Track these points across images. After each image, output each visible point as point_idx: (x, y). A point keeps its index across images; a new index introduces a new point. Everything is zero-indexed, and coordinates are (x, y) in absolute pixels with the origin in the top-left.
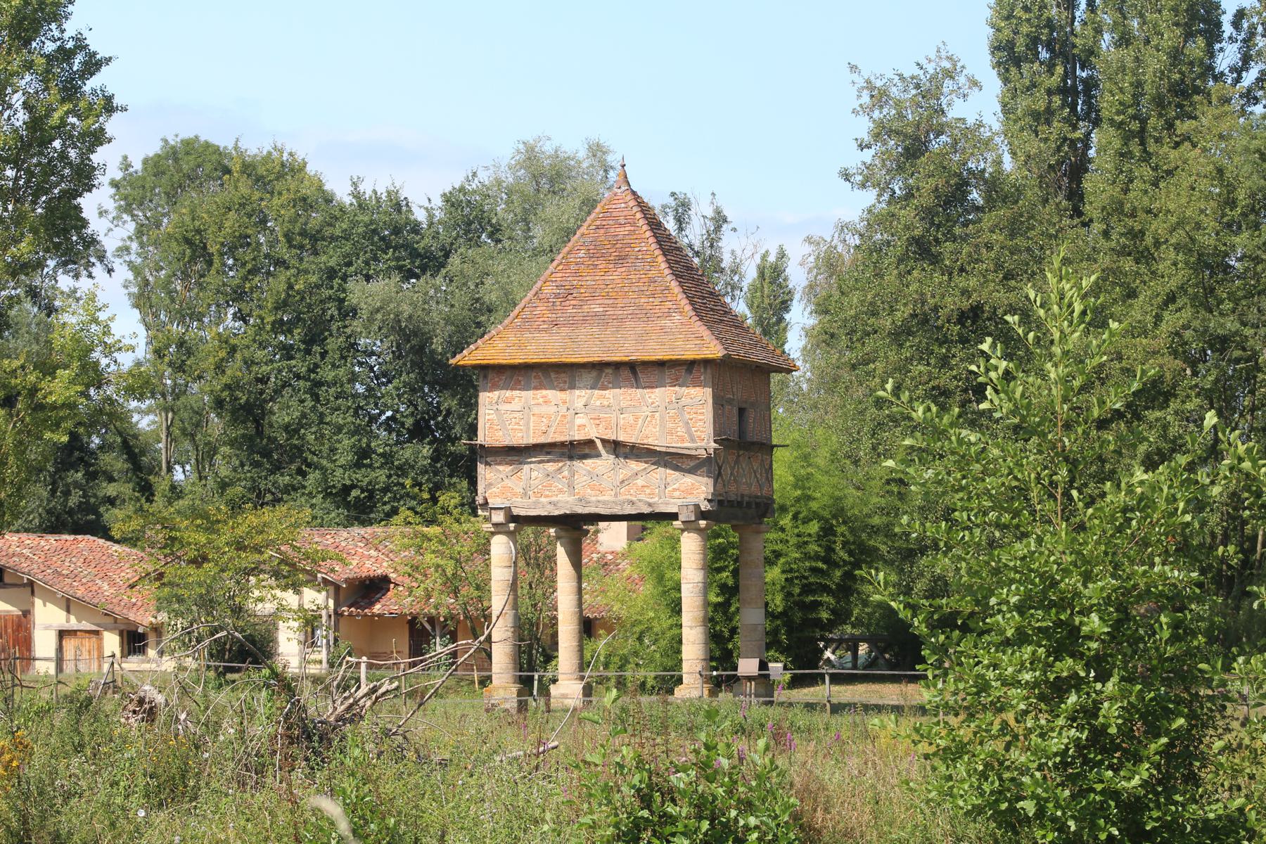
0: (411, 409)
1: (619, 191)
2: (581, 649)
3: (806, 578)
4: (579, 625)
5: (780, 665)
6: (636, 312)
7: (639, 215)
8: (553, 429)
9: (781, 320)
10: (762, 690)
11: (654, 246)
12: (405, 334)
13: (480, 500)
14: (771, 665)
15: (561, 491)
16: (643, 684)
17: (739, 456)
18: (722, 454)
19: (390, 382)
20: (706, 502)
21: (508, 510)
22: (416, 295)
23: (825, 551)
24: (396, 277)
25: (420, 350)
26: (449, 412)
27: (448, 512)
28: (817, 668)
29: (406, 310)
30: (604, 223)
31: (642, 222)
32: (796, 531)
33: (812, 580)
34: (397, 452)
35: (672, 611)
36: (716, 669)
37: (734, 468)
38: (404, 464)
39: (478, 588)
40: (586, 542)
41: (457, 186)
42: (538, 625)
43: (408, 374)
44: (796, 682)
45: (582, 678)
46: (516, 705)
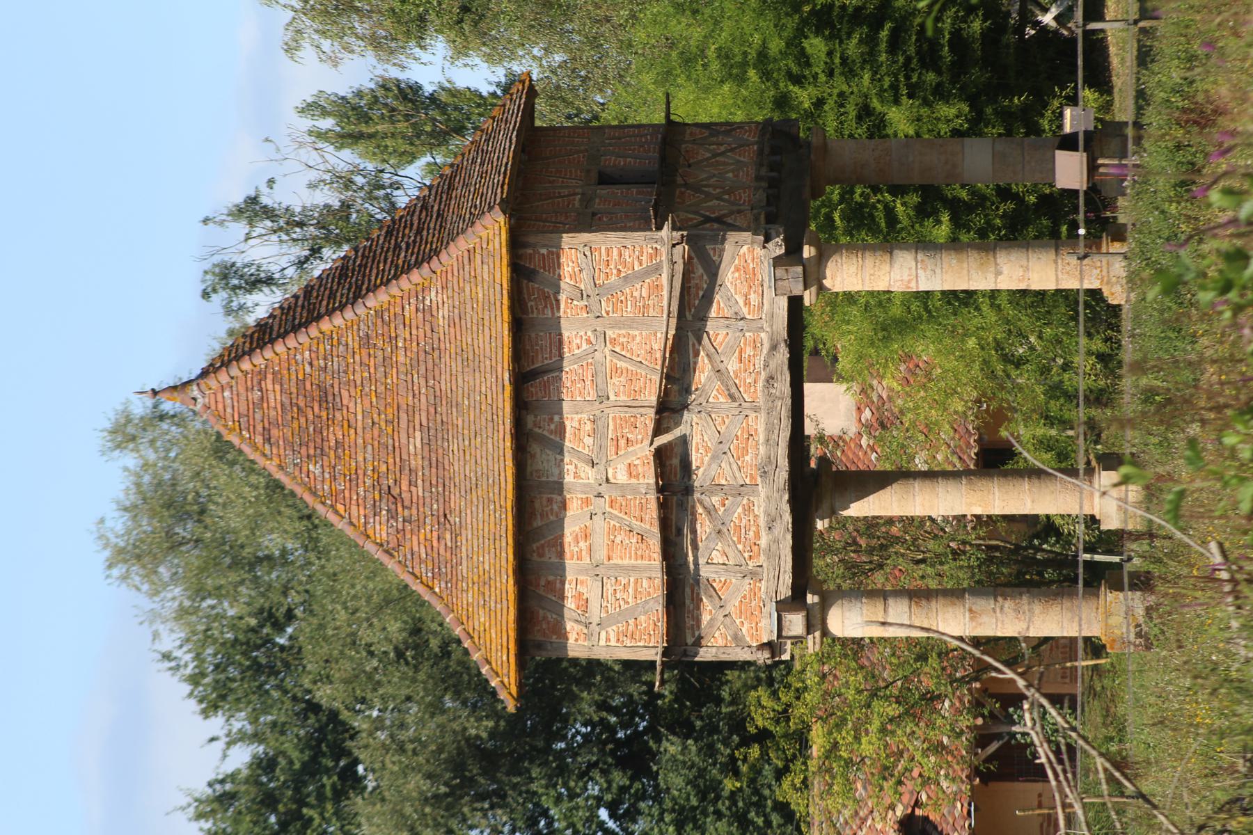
0: (596, 774)
1: (200, 400)
2: (1035, 474)
3: (908, 60)
4: (991, 476)
5: (1068, 112)
6: (422, 371)
7: (246, 365)
8: (636, 524)
9: (433, 98)
10: (1114, 144)
11: (302, 338)
12: (461, 786)
13: (763, 657)
14: (1068, 129)
15: (748, 510)
16: (1101, 357)
17: (686, 185)
18: (683, 215)
19: (545, 813)
20: (770, 245)
21: (783, 607)
22: (389, 765)
23: (860, 25)
24: (358, 803)
25: (488, 758)
26: (603, 706)
27: (785, 711)
28: (1073, 41)
29: (416, 784)
30: (259, 428)
31: (258, 360)
32: (822, 78)
33: (912, 50)
34: (673, 799)
35: (966, 305)
36: (1074, 226)
37: (708, 195)
38: (695, 786)
39: (922, 658)
40: (843, 460)
41: (187, 688)
42: (989, 547)
43: (532, 780)
44: (1100, 78)
45: (1090, 472)
46: (1139, 593)
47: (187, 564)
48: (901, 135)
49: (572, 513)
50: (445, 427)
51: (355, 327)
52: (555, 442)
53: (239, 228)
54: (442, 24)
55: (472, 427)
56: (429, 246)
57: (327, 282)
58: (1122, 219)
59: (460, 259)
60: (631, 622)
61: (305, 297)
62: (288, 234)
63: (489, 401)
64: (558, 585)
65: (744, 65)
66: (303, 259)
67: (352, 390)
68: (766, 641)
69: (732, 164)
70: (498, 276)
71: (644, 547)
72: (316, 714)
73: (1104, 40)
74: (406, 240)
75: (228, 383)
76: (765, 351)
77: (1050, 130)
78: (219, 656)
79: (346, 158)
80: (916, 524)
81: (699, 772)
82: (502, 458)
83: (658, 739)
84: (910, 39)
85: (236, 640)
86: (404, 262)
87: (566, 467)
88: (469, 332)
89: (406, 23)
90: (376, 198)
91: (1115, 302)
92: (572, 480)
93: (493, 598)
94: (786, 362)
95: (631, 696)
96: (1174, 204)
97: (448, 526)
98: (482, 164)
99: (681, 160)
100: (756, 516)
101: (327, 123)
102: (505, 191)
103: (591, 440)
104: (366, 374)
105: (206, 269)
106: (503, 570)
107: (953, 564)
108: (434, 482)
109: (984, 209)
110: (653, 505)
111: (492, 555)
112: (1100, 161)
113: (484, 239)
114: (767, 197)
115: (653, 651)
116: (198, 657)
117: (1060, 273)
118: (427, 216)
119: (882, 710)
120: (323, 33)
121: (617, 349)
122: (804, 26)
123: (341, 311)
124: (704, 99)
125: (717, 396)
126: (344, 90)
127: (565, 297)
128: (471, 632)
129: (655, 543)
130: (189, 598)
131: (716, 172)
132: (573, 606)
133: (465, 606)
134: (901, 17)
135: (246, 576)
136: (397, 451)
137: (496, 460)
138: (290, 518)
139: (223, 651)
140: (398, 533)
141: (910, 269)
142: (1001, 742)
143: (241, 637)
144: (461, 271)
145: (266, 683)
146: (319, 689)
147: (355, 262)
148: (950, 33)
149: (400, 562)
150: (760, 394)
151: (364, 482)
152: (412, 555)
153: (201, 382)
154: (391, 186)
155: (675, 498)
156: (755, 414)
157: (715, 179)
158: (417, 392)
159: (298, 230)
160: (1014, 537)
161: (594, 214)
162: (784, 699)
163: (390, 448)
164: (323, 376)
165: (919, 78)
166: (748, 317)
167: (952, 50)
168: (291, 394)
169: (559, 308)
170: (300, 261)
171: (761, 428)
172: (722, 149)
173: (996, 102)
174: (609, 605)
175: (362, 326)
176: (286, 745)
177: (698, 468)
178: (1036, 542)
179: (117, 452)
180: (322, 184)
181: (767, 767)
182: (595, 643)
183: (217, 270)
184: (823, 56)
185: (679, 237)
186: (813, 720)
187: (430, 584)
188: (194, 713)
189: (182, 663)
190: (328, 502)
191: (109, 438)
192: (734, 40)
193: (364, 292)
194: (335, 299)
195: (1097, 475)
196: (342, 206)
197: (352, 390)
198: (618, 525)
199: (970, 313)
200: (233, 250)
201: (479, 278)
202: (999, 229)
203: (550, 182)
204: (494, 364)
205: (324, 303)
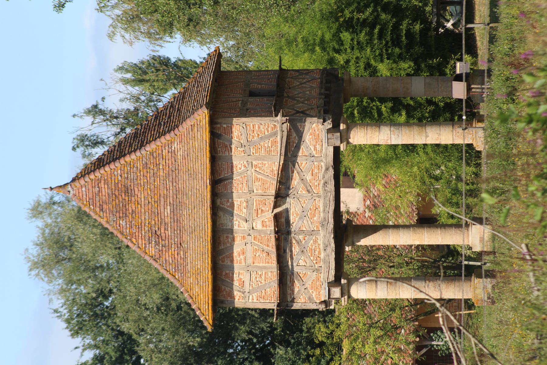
1: (72, 192)
2: (444, 226)
3: (387, 42)
4: (423, 227)
5: (458, 64)
6: (171, 179)
7: (92, 176)
8: (265, 248)
9: (175, 65)
10: (479, 79)
11: (117, 164)
13: (322, 307)
14: (458, 72)
15: (315, 241)
17: (288, 97)
18: (287, 110)
20: (326, 124)
21: (331, 285)
22: (154, 359)
23: (366, 27)
26: (250, 333)
27: (331, 333)
30: (98, 204)
31: (98, 174)
32: (349, 50)
33: (389, 38)
35: (413, 152)
36: (460, 117)
37: (298, 101)
39: (393, 310)
40: (357, 221)
41: (65, 325)
44: (472, 50)
45: (467, 225)
46: (489, 280)
47: (65, 269)
48: (384, 76)
49: (237, 243)
50: (181, 204)
51: (141, 159)
52: (230, 211)
53: (89, 119)
54: (180, 27)
55: (193, 204)
56: (174, 123)
57: (128, 140)
58: (482, 113)
59: (188, 129)
60: (263, 291)
61: (118, 146)
62: (111, 122)
63: (201, 193)
64: (231, 275)
65: (314, 44)
66: (117, 133)
67: (139, 188)
68: (323, 300)
69: (309, 88)
70: (204, 137)
71: (269, 258)
72: (122, 336)
73: (474, 34)
74: (163, 121)
75: (84, 184)
76: (323, 171)
77: (450, 74)
78: (79, 310)
79: (136, 90)
80: (390, 250)
81: (293, 363)
82: (206, 218)
83: (275, 348)
84: (388, 33)
85: (87, 303)
86: (163, 131)
87: (235, 222)
88: (192, 161)
89: (164, 26)
90: (150, 106)
91: (479, 150)
92: (237, 228)
93: (202, 280)
94: (333, 176)
95: (263, 328)
96: (505, 105)
97: (182, 248)
98: (198, 87)
99: (286, 85)
100: (319, 244)
101: (129, 76)
102: (208, 99)
103: (246, 210)
104: (146, 181)
105: (74, 137)
106: (206, 268)
107: (406, 268)
108: (176, 229)
109: (421, 109)
110: (273, 240)
111: (201, 261)
112: (472, 86)
113: (198, 120)
114: (324, 102)
115: (273, 304)
116: (70, 311)
117: (454, 137)
118: (173, 110)
119: (374, 333)
120: (126, 30)
121: (258, 170)
122: (340, 28)
123: (135, 152)
124: (296, 60)
125: (302, 191)
126: (135, 61)
127: (234, 146)
128: (192, 296)
129: (274, 256)
130: (66, 284)
131: (302, 91)
132: (237, 284)
133: (189, 284)
134: (384, 23)
135: (91, 274)
136: (159, 215)
137: (203, 219)
138: (110, 248)
139: (81, 308)
140: (159, 251)
141: (388, 134)
142: (427, 349)
143: (89, 302)
144: (188, 134)
145: (99, 322)
146: (123, 325)
147: (141, 131)
148: (406, 30)
149: (160, 264)
150: (321, 190)
151: (145, 229)
152: (166, 261)
153: (72, 184)
154: (157, 101)
155: (283, 236)
156: (319, 199)
157: (301, 94)
158: (168, 188)
159: (115, 120)
160: (433, 256)
161: (247, 110)
162: (331, 328)
163: (156, 213)
164: (126, 181)
165: (392, 51)
166: (315, 155)
167: (406, 38)
168: (112, 189)
169: (231, 152)
170: (116, 134)
171: (321, 205)
172: (305, 81)
173: (426, 61)
174: (253, 284)
175: (144, 159)
176: (109, 350)
177: (293, 223)
178: (443, 259)
179: (34, 219)
180: (126, 99)
181: (323, 360)
182: (247, 301)
183: (79, 138)
184: (349, 41)
185: (285, 120)
186: (344, 337)
187: (174, 274)
188: (68, 336)
189: (63, 314)
190: (129, 238)
191: (30, 213)
192: (309, 33)
193: (145, 144)
194: (132, 147)
195: (470, 227)
196: (135, 110)
197: (139, 188)
198: (257, 248)
199: (414, 155)
200: (86, 129)
201: (196, 138)
202: (428, 118)
203: (228, 95)
204: (203, 176)
205: (127, 149)
